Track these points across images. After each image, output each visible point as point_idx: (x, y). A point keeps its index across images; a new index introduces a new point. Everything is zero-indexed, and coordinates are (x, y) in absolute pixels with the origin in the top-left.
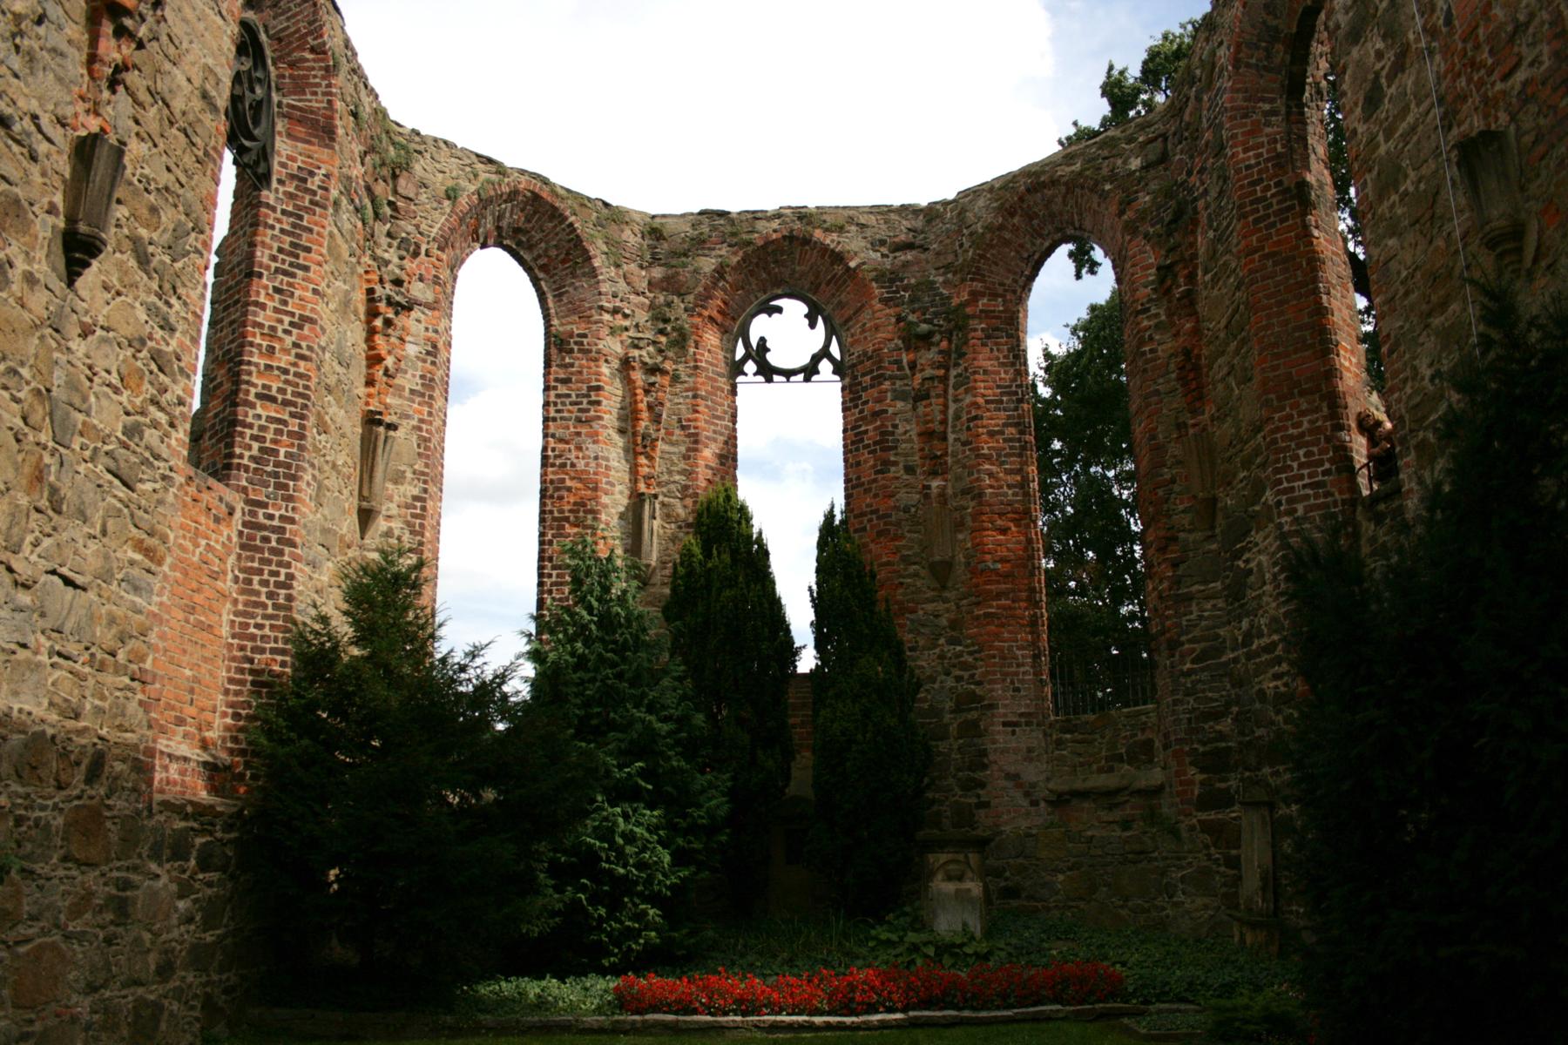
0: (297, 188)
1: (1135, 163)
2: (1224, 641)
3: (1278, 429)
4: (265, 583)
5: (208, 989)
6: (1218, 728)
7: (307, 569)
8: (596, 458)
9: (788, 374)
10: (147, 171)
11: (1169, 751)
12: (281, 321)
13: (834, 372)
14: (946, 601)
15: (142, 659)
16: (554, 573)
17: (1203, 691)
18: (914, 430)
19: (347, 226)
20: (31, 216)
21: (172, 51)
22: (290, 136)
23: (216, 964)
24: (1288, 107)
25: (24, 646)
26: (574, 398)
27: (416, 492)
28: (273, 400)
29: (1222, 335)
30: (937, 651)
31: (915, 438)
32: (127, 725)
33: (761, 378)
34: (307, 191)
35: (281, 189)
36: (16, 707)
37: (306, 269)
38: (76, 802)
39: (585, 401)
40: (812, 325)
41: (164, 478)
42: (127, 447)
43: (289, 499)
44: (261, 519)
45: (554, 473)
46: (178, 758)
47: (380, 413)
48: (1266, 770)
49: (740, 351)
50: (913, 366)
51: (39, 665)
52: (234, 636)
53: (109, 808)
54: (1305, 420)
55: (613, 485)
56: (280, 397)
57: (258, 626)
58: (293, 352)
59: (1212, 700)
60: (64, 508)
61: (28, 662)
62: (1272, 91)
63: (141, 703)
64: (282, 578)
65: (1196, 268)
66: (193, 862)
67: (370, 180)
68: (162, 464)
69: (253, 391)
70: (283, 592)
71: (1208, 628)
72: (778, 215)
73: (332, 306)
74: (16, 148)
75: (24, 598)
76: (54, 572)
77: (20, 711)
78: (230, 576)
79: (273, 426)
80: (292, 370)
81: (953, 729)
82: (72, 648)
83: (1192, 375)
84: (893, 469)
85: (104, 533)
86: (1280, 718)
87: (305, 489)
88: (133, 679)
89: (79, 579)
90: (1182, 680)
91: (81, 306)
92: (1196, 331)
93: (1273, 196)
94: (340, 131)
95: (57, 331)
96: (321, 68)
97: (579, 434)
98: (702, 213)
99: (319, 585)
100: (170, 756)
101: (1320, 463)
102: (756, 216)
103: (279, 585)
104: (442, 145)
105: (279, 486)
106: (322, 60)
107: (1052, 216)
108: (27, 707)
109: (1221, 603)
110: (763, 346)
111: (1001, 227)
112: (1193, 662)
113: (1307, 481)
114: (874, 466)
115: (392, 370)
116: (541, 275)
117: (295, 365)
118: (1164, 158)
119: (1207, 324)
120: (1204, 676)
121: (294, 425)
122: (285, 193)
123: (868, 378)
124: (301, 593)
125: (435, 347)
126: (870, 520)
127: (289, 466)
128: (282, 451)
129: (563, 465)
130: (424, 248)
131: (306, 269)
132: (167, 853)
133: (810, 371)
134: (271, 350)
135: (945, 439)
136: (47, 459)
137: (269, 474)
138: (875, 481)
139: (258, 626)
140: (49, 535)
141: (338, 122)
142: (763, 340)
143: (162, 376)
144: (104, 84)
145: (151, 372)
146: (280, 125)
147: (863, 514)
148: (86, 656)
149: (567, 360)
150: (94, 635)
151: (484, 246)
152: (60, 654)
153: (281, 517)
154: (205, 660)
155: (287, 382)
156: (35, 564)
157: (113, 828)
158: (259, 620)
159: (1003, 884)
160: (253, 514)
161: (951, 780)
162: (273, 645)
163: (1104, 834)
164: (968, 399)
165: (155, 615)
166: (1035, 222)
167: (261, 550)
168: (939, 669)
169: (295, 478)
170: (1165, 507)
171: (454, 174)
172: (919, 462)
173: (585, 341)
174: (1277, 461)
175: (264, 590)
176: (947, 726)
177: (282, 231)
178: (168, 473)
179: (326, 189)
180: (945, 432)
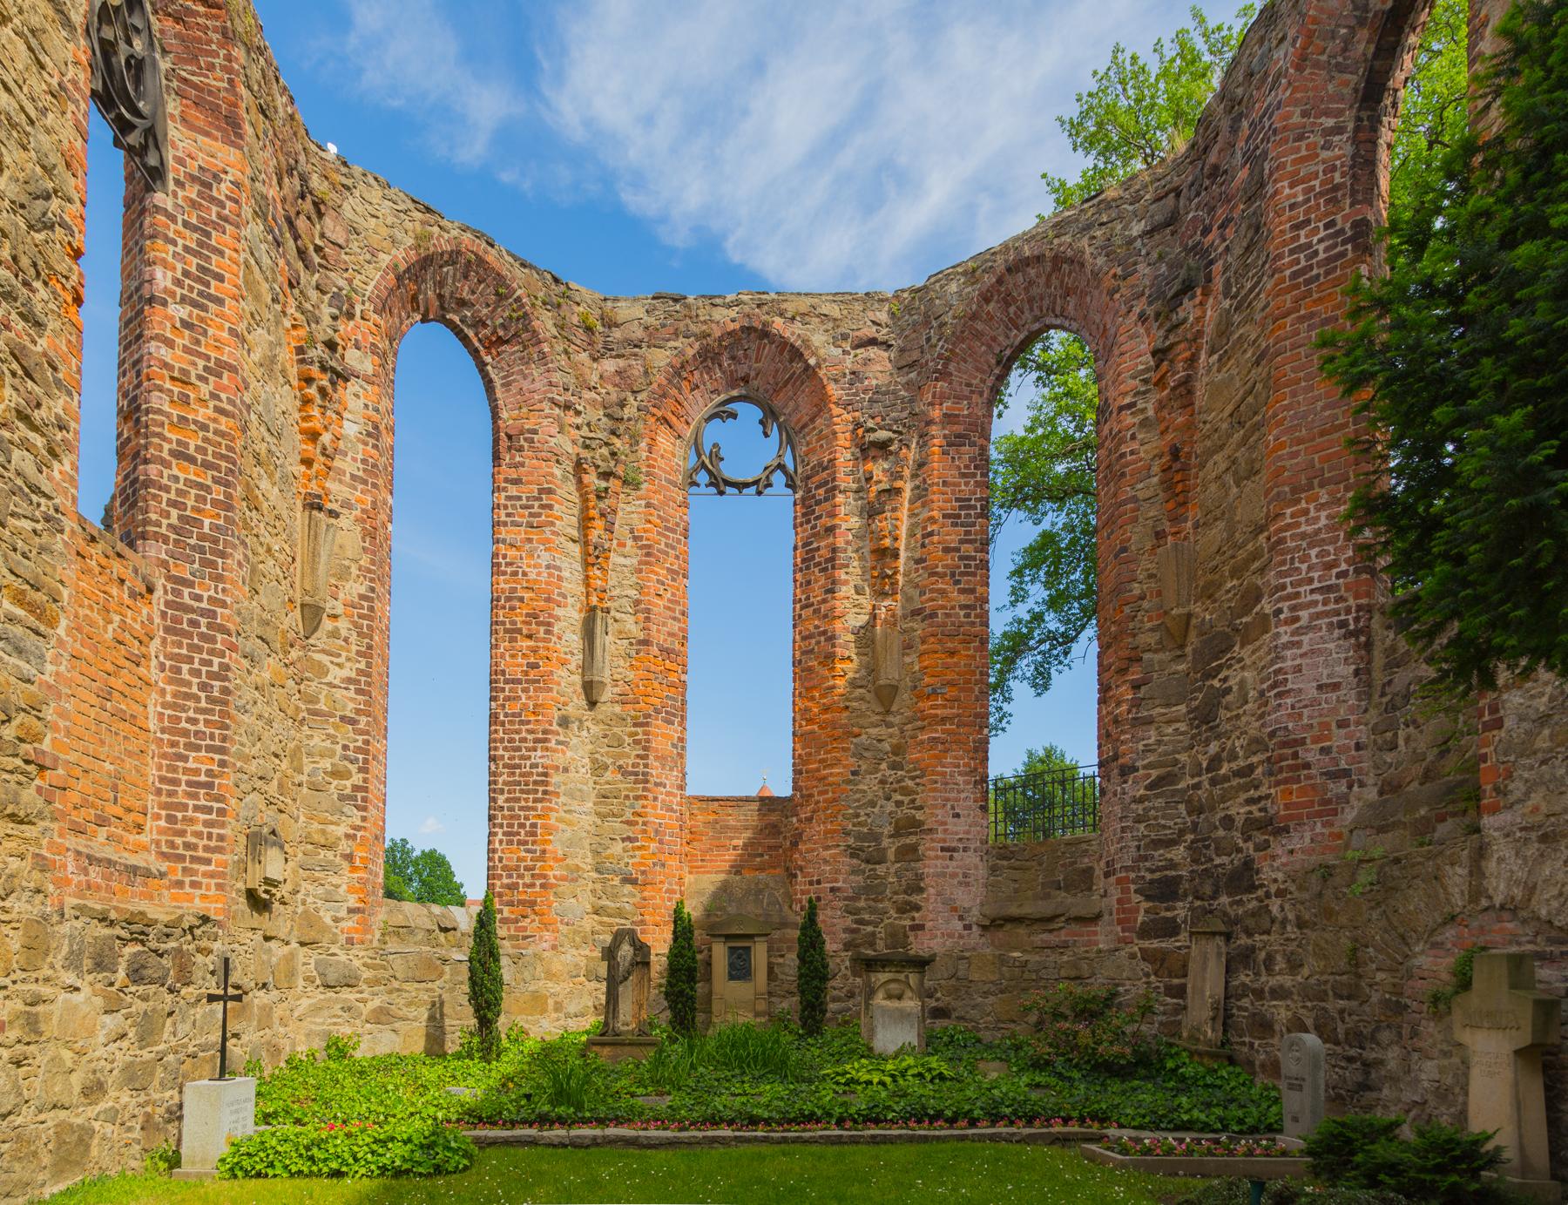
0: (200, 194)
1: (1137, 228)
2: (1183, 767)
3: (1289, 527)
4: (197, 673)
5: (149, 1109)
6: (1169, 856)
7: (245, 663)
8: (548, 567)
9: (741, 486)
11: (1112, 879)
14: (889, 725)
15: (38, 738)
16: (507, 687)
17: (1156, 818)
19: (266, 261)
23: (156, 1082)
24: (1359, 119)
27: (363, 590)
28: (192, 460)
29: (1225, 426)
32: (22, 814)
33: (713, 490)
34: (213, 200)
35: (180, 193)
37: (220, 302)
39: (536, 504)
41: (47, 519)
44: (187, 600)
45: (506, 582)
46: (99, 861)
48: (1224, 899)
52: (163, 731)
54: (1323, 514)
56: (199, 457)
58: (211, 404)
59: (1164, 827)
62: (1342, 100)
63: (39, 790)
64: (215, 668)
65: (1199, 349)
69: (166, 446)
70: (216, 683)
71: (1166, 754)
78: (154, 662)
79: (193, 491)
80: (212, 426)
81: (891, 854)
83: (1178, 477)
86: (1250, 845)
87: (233, 566)
88: (27, 762)
90: (1133, 806)
92: (1190, 427)
93: (1320, 241)
97: (530, 541)
100: (89, 857)
101: (1334, 564)
103: (211, 675)
106: (217, 17)
109: (1183, 727)
110: (716, 456)
112: (1146, 788)
113: (1316, 585)
115: (330, 451)
116: (488, 359)
117: (215, 420)
118: (1172, 220)
119: (1204, 417)
120: (1160, 802)
121: (218, 493)
122: (186, 198)
123: (821, 491)
124: (238, 687)
125: (376, 427)
126: (818, 643)
128: (207, 522)
129: (515, 574)
130: (358, 308)
131: (220, 302)
132: (87, 963)
134: (185, 400)
137: (193, 548)
143: (30, 383)
145: (14, 374)
146: (173, 106)
149: (518, 459)
151: (424, 320)
153: (210, 598)
154: (130, 754)
155: (205, 440)
158: (191, 714)
159: (934, 1004)
160: (179, 594)
161: (887, 904)
162: (208, 742)
163: (1037, 958)
164: (925, 514)
165: (50, 687)
167: (189, 636)
168: (880, 793)
169: (223, 555)
170: (1131, 625)
171: (389, 221)
173: (536, 437)
174: (1283, 563)
175: (196, 680)
178: (52, 512)
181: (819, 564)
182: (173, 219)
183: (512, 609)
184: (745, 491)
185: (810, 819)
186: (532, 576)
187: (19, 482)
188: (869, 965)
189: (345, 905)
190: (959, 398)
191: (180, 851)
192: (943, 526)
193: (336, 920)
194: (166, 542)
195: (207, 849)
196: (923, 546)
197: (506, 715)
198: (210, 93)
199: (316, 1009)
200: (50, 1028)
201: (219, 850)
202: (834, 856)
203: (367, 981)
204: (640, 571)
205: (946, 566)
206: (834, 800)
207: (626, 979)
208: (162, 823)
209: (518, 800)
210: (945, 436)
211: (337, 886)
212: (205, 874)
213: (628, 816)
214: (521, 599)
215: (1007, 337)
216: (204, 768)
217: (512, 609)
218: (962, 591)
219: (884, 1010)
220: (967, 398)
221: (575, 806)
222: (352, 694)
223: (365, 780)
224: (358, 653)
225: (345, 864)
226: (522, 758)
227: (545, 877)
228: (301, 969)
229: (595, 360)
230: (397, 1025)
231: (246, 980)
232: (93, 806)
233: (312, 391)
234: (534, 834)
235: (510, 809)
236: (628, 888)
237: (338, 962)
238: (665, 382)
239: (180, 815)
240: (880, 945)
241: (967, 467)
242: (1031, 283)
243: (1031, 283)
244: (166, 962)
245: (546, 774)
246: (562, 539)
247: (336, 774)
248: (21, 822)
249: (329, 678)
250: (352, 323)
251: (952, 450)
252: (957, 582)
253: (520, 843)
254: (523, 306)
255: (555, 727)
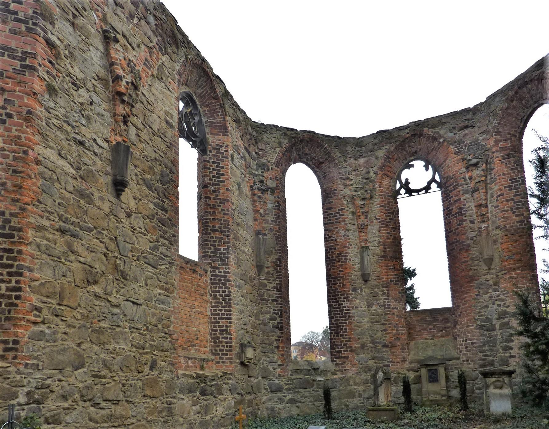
4: (221, 295)
7: (237, 289)
9: (418, 191)
10: (146, 153)
12: (217, 202)
13: (438, 187)
15: (169, 327)
18: (473, 205)
19: (238, 164)
20: (98, 176)
21: (149, 107)
22: (212, 134)
25: (119, 326)
26: (334, 215)
27: (277, 257)
28: (217, 231)
30: (489, 295)
31: (474, 209)
33: (407, 195)
35: (211, 154)
36: (118, 347)
38: (147, 377)
39: (338, 215)
40: (427, 169)
41: (170, 263)
42: (152, 254)
43: (226, 265)
44: (217, 273)
46: (192, 359)
47: (260, 230)
49: (398, 186)
50: (471, 178)
51: (125, 333)
53: (160, 378)
55: (351, 245)
57: (220, 310)
58: (222, 213)
60: (128, 278)
61: (121, 333)
64: (227, 293)
66: (198, 393)
67: (247, 145)
68: (168, 259)
72: (408, 127)
73: (236, 194)
74: (88, 152)
75: (116, 310)
76: (127, 300)
77: (120, 348)
78: (208, 294)
81: (497, 327)
82: (138, 326)
84: (465, 223)
85: (146, 285)
89: (138, 302)
91: (124, 206)
94: (230, 128)
95: (116, 216)
96: (218, 105)
98: (378, 132)
99: (242, 294)
102: (399, 129)
103: (226, 295)
104: (273, 127)
105: (222, 261)
106: (218, 102)
107: (532, 96)
108: (122, 347)
111: (507, 108)
114: (457, 222)
117: (223, 217)
124: (234, 297)
125: (278, 203)
126: (456, 245)
127: (225, 254)
128: (222, 248)
133: (427, 189)
135: (486, 206)
136: (118, 262)
137: (218, 257)
138: (457, 229)
139: (220, 310)
140: (123, 288)
141: (228, 125)
142: (407, 180)
144: (122, 124)
145: (159, 226)
147: (453, 243)
148: (145, 328)
150: (147, 320)
152: (133, 328)
155: (221, 224)
156: (119, 298)
157: (163, 384)
158: (220, 308)
160: (214, 272)
165: (172, 311)
166: (524, 102)
168: (490, 302)
169: (228, 257)
171: (279, 137)
172: (476, 218)
176: (494, 325)
177: (213, 169)
179: (227, 151)
180: (486, 204)
181: (454, 215)
182: (209, 162)
183: (332, 252)
184: (420, 193)
185: (460, 315)
186: (339, 240)
187: (161, 256)
188: (486, 375)
189: (277, 364)
190: (506, 140)
191: (218, 352)
192: (505, 191)
193: (274, 369)
194: (210, 257)
195: (226, 350)
196: (497, 200)
197: (332, 290)
198: (218, 123)
199: (270, 400)
200: (176, 411)
201: (231, 351)
202: (471, 330)
203: (286, 389)
204: (380, 231)
205: (508, 207)
206: (469, 307)
207: (381, 385)
208: (212, 344)
209: (339, 320)
210: (501, 156)
211: (274, 357)
212: (226, 359)
213: (383, 322)
214: (335, 249)
215: (523, 112)
216: (224, 325)
217: (332, 252)
218: (517, 216)
219: (495, 394)
220: (509, 139)
221: (361, 320)
222: (275, 292)
223: (281, 320)
224: (277, 278)
225: (276, 350)
226: (339, 305)
227: (351, 347)
228: (262, 386)
229: (356, 160)
230: (297, 404)
231: (242, 391)
232: (190, 341)
233: (255, 198)
234: (346, 332)
235: (336, 324)
236: (385, 349)
237: (276, 384)
238: (383, 161)
239: (218, 341)
240: (496, 364)
241: (512, 166)
242: (530, 90)
243: (530, 90)
244: (213, 389)
245: (348, 310)
246: (349, 225)
247: (272, 319)
248: (165, 351)
249: (268, 288)
250: (269, 173)
251: (505, 161)
252: (515, 212)
253: (341, 336)
254: (327, 150)
255: (351, 292)
